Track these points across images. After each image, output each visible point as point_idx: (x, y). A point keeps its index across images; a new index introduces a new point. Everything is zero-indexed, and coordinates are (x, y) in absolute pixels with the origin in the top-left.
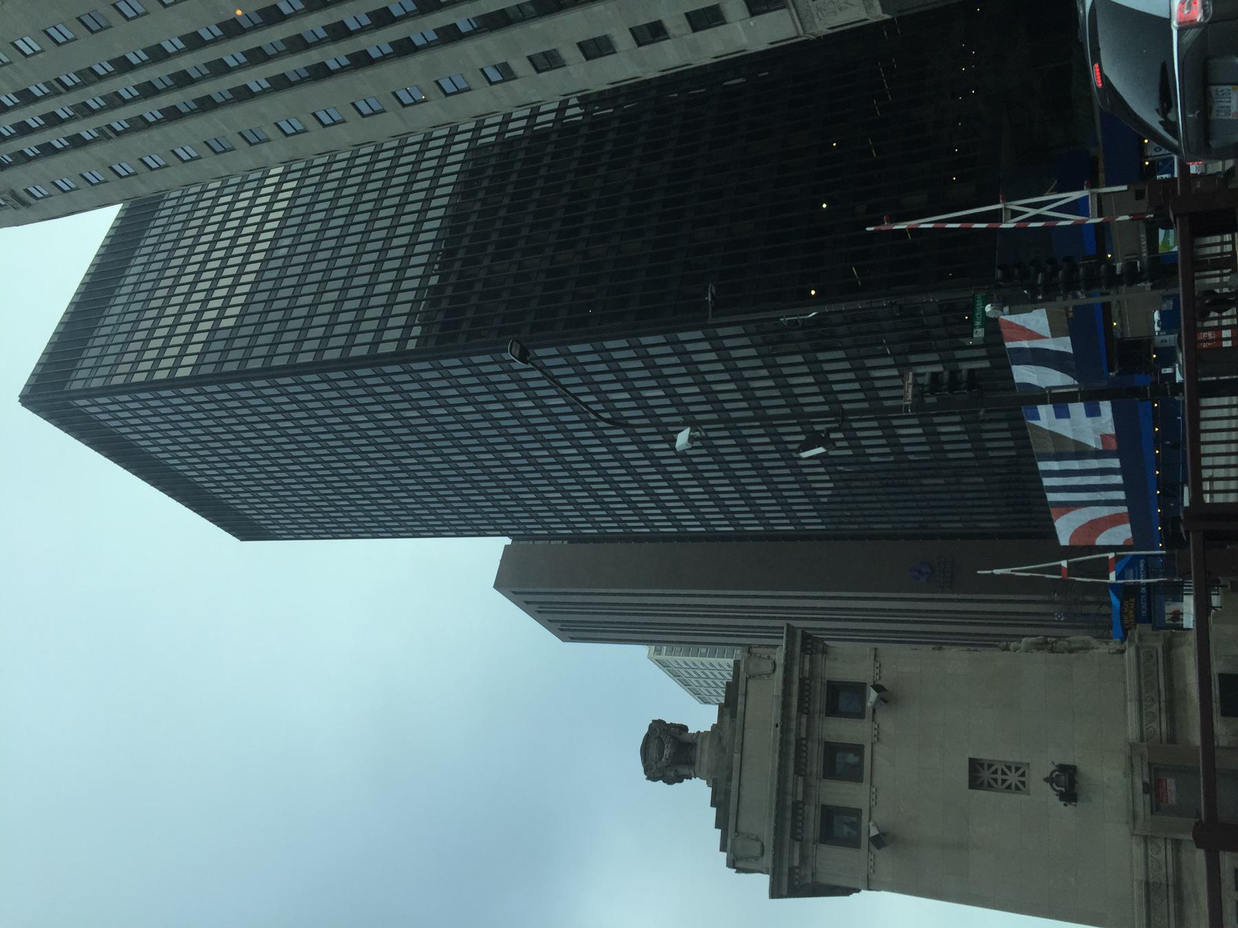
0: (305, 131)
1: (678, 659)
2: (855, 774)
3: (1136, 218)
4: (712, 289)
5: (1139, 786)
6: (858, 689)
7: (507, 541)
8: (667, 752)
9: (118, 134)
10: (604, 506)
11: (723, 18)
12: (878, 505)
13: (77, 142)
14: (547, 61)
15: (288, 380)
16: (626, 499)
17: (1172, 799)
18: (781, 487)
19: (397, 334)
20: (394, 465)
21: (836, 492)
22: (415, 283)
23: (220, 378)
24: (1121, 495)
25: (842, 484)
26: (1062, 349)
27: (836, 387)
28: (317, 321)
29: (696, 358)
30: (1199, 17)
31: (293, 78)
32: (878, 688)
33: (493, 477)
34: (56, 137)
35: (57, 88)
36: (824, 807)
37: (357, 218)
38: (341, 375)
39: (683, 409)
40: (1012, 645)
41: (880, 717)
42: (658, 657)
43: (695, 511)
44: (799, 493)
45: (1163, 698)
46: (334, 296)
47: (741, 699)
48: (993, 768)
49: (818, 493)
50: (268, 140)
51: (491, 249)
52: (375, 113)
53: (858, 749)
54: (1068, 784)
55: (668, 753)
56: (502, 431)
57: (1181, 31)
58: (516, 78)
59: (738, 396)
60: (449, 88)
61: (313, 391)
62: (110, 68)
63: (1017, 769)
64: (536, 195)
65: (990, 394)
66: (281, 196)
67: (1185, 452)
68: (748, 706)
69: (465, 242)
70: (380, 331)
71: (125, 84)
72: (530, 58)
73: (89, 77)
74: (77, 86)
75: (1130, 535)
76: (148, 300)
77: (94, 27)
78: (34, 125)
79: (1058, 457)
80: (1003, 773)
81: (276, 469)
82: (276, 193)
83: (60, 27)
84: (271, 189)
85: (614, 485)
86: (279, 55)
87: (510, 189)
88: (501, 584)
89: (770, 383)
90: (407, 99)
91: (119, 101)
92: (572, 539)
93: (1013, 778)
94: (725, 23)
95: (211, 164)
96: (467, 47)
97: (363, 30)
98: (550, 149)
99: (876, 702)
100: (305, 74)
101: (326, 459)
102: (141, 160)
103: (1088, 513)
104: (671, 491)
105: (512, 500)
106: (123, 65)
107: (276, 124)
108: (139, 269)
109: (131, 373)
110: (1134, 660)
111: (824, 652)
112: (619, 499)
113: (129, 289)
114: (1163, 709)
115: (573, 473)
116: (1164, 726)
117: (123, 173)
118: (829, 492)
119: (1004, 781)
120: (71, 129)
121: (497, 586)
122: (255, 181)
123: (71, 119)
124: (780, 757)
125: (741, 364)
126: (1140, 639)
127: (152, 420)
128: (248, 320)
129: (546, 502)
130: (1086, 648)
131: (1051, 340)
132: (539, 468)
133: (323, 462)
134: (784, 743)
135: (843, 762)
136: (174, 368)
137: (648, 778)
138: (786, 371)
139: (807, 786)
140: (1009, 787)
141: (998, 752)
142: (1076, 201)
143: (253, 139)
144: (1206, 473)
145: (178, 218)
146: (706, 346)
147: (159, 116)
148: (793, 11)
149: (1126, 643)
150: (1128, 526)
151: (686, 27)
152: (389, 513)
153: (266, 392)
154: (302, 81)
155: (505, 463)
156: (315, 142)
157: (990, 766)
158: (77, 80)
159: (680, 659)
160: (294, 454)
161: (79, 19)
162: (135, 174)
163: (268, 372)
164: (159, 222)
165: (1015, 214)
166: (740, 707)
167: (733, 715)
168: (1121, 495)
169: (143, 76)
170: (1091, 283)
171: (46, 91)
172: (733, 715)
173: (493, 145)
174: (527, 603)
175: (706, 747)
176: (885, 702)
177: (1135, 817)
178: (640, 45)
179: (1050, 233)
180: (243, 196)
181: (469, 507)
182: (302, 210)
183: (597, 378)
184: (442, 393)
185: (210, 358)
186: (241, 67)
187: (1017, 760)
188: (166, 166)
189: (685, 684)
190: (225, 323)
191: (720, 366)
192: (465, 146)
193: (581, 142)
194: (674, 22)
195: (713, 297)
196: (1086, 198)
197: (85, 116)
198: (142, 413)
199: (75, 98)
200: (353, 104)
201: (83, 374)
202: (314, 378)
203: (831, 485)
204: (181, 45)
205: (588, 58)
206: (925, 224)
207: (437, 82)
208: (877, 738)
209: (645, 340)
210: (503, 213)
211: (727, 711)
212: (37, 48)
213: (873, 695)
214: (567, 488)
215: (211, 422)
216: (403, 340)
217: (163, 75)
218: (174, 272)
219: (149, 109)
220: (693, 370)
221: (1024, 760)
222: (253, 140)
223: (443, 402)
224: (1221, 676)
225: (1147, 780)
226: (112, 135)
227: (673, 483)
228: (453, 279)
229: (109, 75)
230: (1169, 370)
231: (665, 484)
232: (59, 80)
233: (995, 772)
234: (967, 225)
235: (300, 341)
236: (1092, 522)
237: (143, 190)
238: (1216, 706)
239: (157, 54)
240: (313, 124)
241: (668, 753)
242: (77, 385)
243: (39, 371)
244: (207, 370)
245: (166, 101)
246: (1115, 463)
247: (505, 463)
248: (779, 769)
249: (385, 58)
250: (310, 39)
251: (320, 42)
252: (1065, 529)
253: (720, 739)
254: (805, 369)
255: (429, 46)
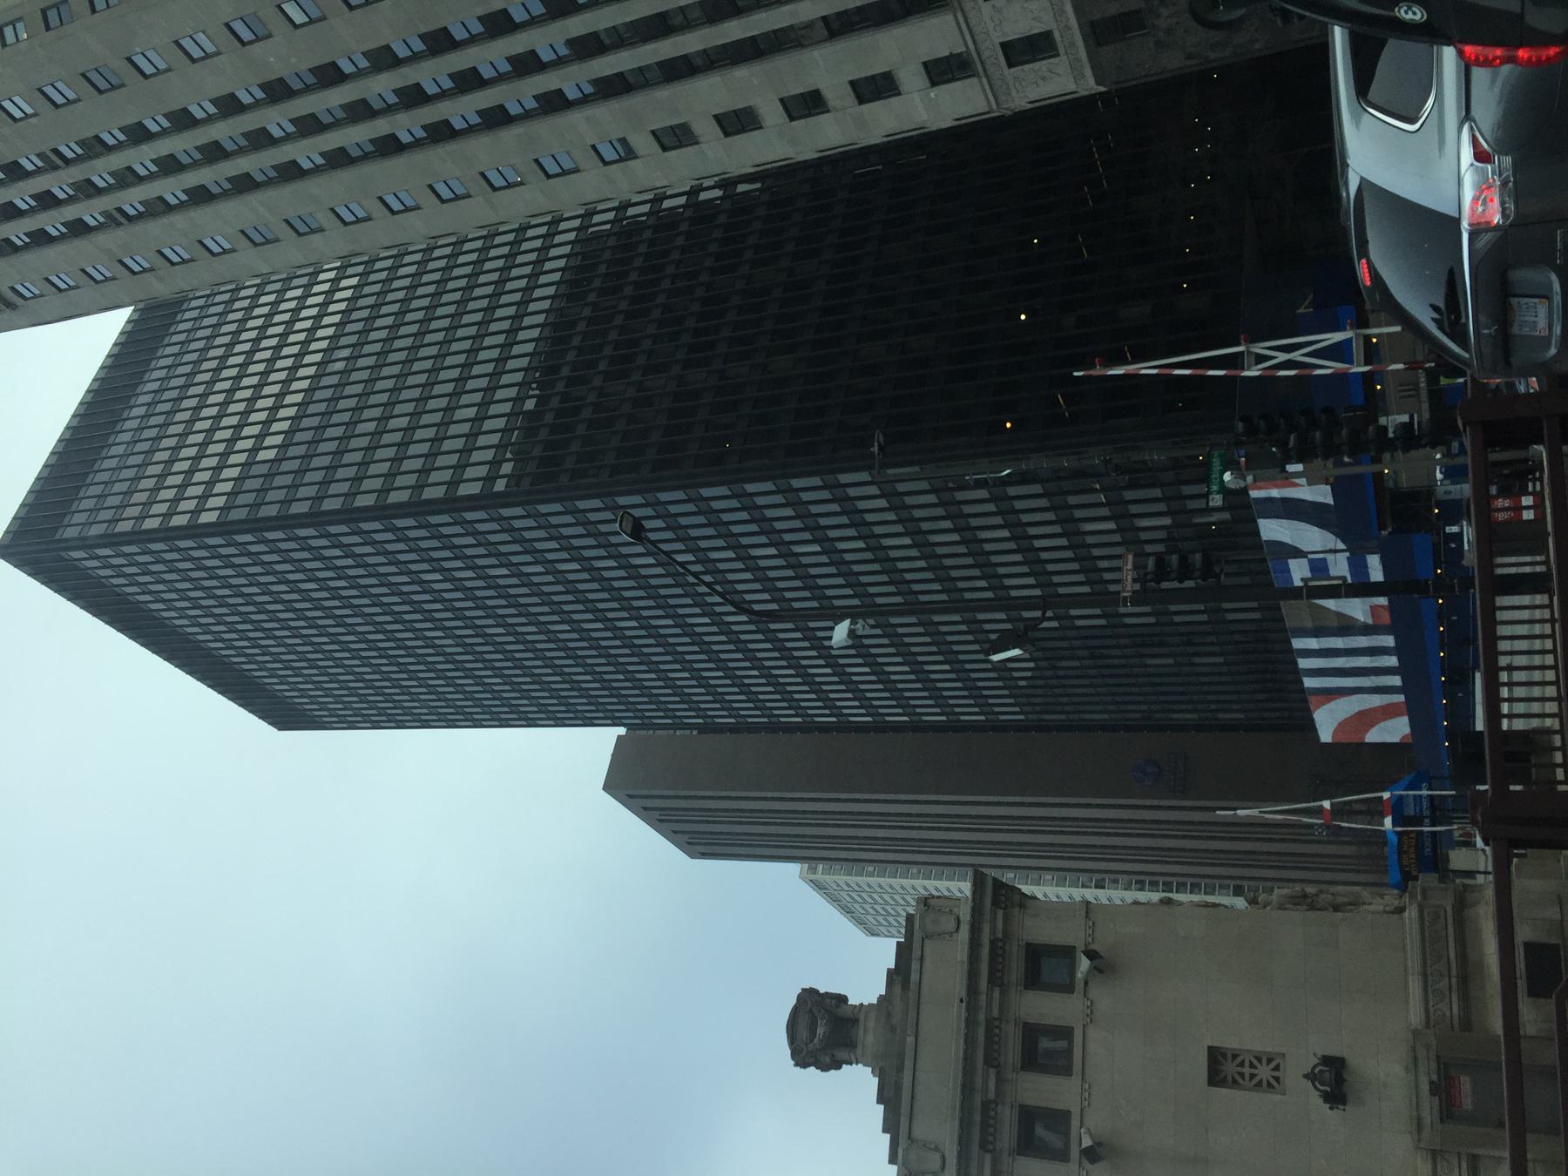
0: (368, 219)
1: (839, 879)
2: (1060, 1064)
3: (1413, 366)
4: (879, 437)
5: (1425, 1088)
6: (1068, 953)
7: (622, 731)
8: (820, 1031)
9: (129, 218)
10: (745, 689)
11: (897, 88)
12: (1092, 691)
13: (78, 228)
14: (676, 137)
15: (343, 529)
16: (772, 681)
17: (1467, 1103)
18: (968, 666)
19: (482, 471)
20: (477, 636)
21: (1037, 673)
22: (506, 408)
23: (255, 525)
24: (1396, 681)
25: (1044, 664)
26: (1320, 499)
27: (1038, 544)
28: (380, 454)
29: (861, 505)
30: (1497, 219)
31: (355, 152)
32: (1091, 955)
33: (603, 652)
34: (52, 221)
35: (54, 161)
36: (1022, 1107)
37: (435, 325)
38: (411, 522)
39: (844, 568)
40: (1262, 898)
41: (1094, 992)
42: (812, 877)
43: (859, 695)
44: (992, 675)
45: (1454, 972)
46: (403, 422)
47: (915, 966)
48: (1239, 1059)
49: (1015, 674)
50: (321, 230)
51: (602, 366)
52: (457, 198)
53: (1065, 1033)
54: (1334, 1081)
55: (822, 1030)
56: (616, 595)
57: (1473, 236)
58: (636, 157)
59: (914, 553)
60: (552, 168)
61: (373, 543)
62: (122, 137)
63: (1270, 1061)
64: (661, 299)
65: (1227, 557)
66: (338, 295)
67: (1476, 650)
68: (925, 976)
69: (571, 356)
70: (461, 467)
71: (142, 158)
72: (653, 132)
73: (95, 147)
74: (79, 159)
75: (1407, 730)
76: (187, 386)
77: (103, 85)
78: (24, 207)
79: (1318, 632)
80: (1252, 1066)
81: (325, 639)
82: (326, 304)
83: (59, 85)
84: (326, 287)
85: (757, 663)
86: (337, 124)
87: (628, 291)
88: (607, 787)
89: (955, 537)
90: (498, 182)
91: (131, 178)
92: (702, 729)
93: (1264, 1072)
94: (899, 94)
95: (249, 259)
96: (576, 119)
97: (443, 95)
98: (680, 241)
99: (1089, 971)
100: (370, 148)
101: (389, 627)
102: (160, 252)
103: (1353, 695)
104: (829, 671)
105: (626, 680)
106: (138, 134)
107: (332, 210)
108: (155, 386)
109: (142, 518)
110: (1416, 926)
111: (1022, 906)
112: (763, 681)
113: (141, 411)
114: (1454, 986)
115: (705, 647)
116: (1455, 1008)
117: (136, 268)
118: (1029, 674)
119: (1252, 1076)
120: (70, 213)
121: (607, 788)
122: (304, 276)
123: (71, 200)
124: (966, 1042)
125: (918, 513)
126: (1424, 896)
127: (167, 577)
128: (299, 437)
129: (669, 683)
130: (1356, 903)
131: (1306, 488)
132: (662, 641)
133: (385, 632)
134: (970, 1023)
135: (1046, 1050)
136: (196, 512)
137: (796, 1065)
138: (974, 522)
139: (1000, 1080)
140: (1259, 1084)
141: (1244, 1037)
142: (1340, 343)
143: (303, 229)
144: (1503, 661)
145: (206, 322)
146: (874, 490)
147: (184, 197)
148: (984, 80)
149: (1406, 898)
150: (1405, 719)
151: (850, 98)
152: (469, 696)
153: (314, 543)
154: (365, 157)
155: (618, 634)
156: (381, 234)
157: (1235, 1056)
158: (80, 151)
159: (842, 879)
160: (349, 620)
161: (84, 75)
162: (152, 270)
163: (316, 518)
164: (176, 338)
165: (1261, 359)
166: (914, 976)
167: (905, 986)
168: (1396, 681)
169: (164, 147)
170: (1357, 448)
171: (40, 164)
172: (905, 986)
173: (608, 234)
174: (645, 809)
175: (871, 1024)
176: (1101, 971)
177: (1415, 1059)
178: (792, 119)
179: (1306, 383)
180: (289, 294)
181: (577, 665)
182: (377, 288)
183: (735, 529)
184: (538, 545)
185: (242, 499)
186: (288, 137)
187: (1269, 1049)
188: (192, 260)
189: (847, 911)
190: (263, 455)
191: (891, 516)
192: (571, 236)
193: (718, 234)
194: (836, 91)
195: (881, 448)
196: (1349, 341)
197: (89, 197)
198: (154, 568)
199: (76, 174)
200: (430, 186)
201: (80, 518)
202: (376, 525)
203: (1031, 665)
204: (212, 109)
205: (727, 134)
206: (1147, 369)
207: (537, 161)
208: (1090, 1016)
209: (797, 483)
210: (618, 321)
211: (898, 979)
212: (29, 111)
213: (1084, 964)
214: (696, 666)
215: (242, 581)
216: (490, 479)
217: (189, 146)
218: (220, 352)
219: (172, 189)
220: (858, 521)
221: (1277, 1050)
222: (302, 229)
223: (539, 557)
224: (1527, 945)
225: (1435, 1077)
226: (122, 220)
227: (831, 661)
228: (555, 402)
229: (120, 146)
230: (1455, 529)
231: (821, 662)
232: (56, 152)
233: (1242, 1064)
234: (1199, 372)
235: (358, 479)
236: (1361, 715)
237: (161, 289)
238: (1522, 985)
239: (182, 120)
240: (378, 211)
241: (822, 1030)
242: (71, 533)
243: (22, 515)
244: (237, 515)
245: (191, 179)
246: (1389, 641)
247: (618, 634)
248: (965, 1059)
249: (471, 130)
250: (377, 105)
251: (389, 109)
252: (1327, 722)
253: (889, 1015)
254: (998, 520)
255: (527, 115)
